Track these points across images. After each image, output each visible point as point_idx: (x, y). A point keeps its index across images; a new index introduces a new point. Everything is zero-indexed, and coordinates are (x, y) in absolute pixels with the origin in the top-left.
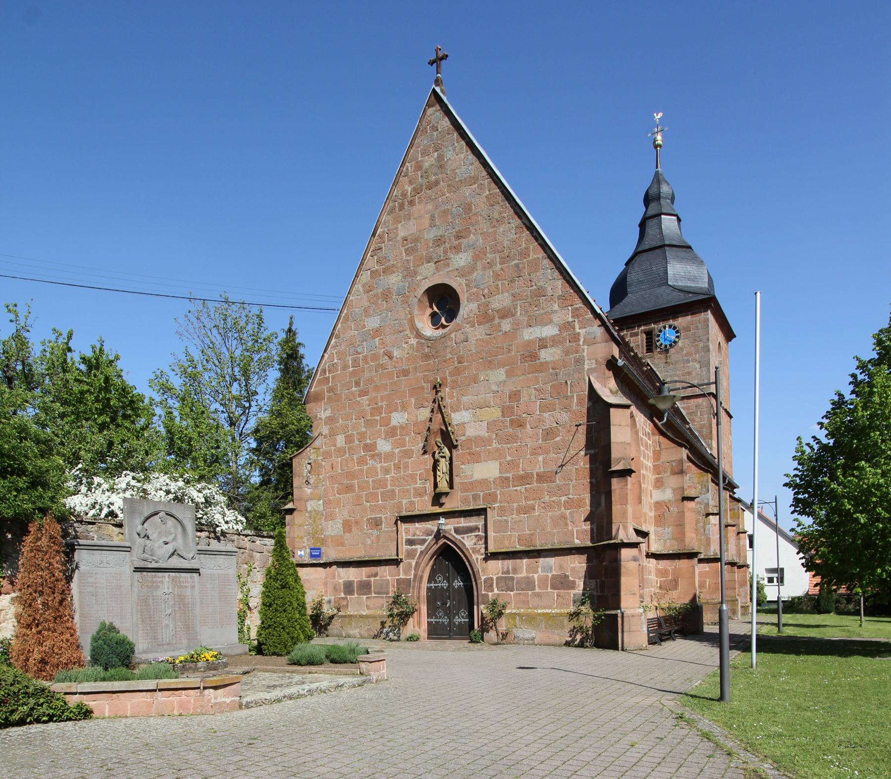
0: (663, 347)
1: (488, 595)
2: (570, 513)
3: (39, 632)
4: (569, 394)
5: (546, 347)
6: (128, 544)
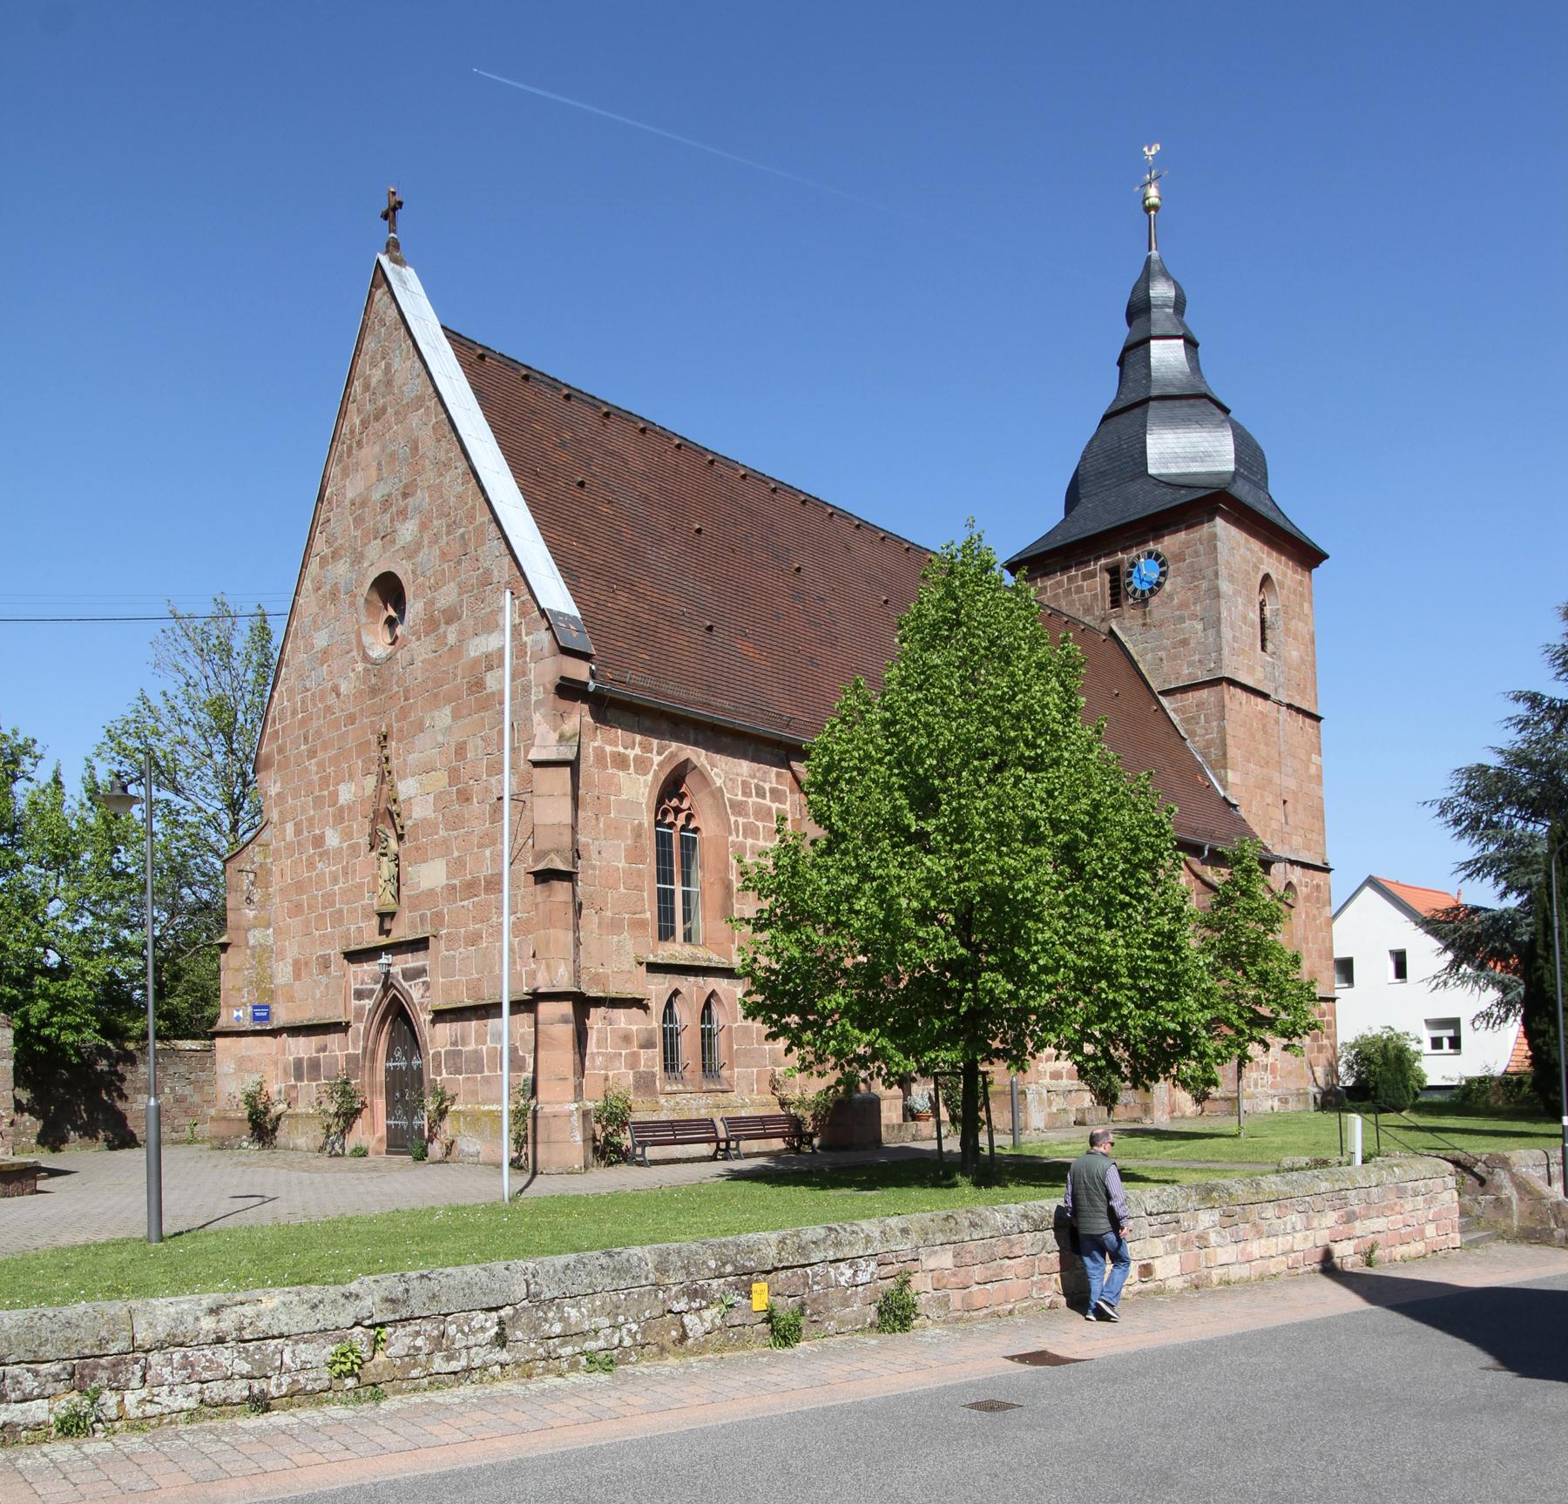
0: (1138, 594)
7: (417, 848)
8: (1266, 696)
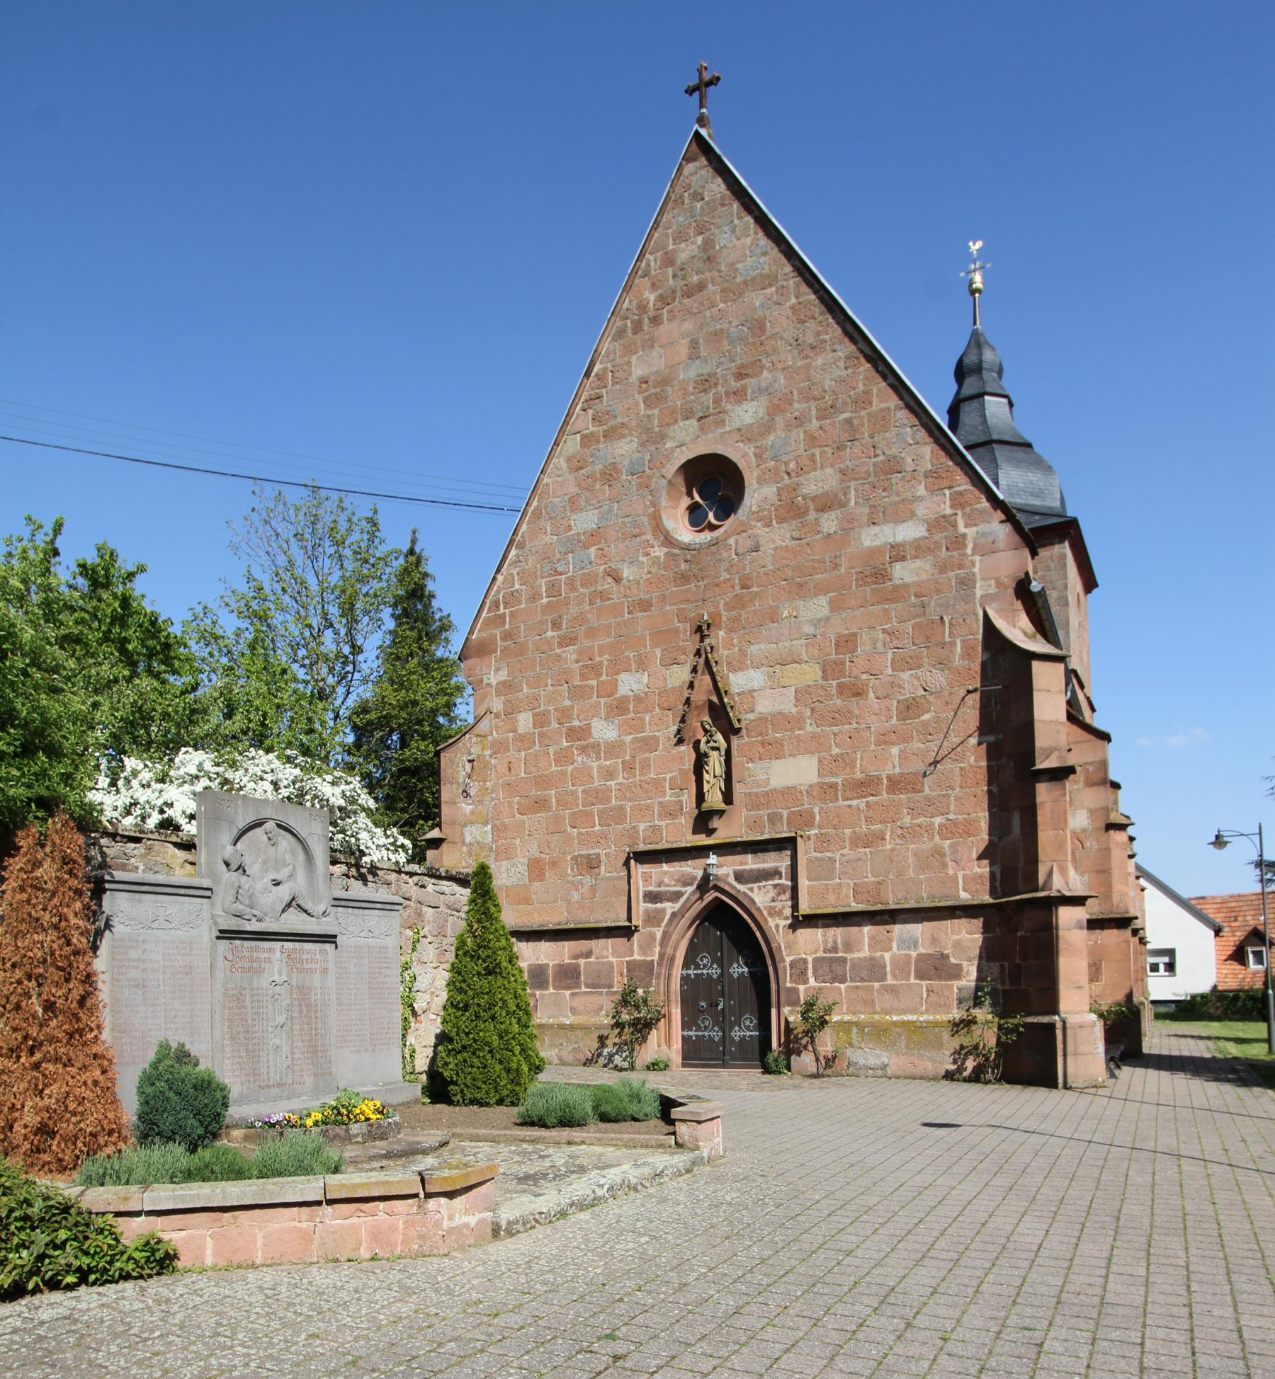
1: (797, 990)
2: (951, 846)
3: (36, 1066)
4: (947, 639)
5: (903, 559)
6: (206, 883)
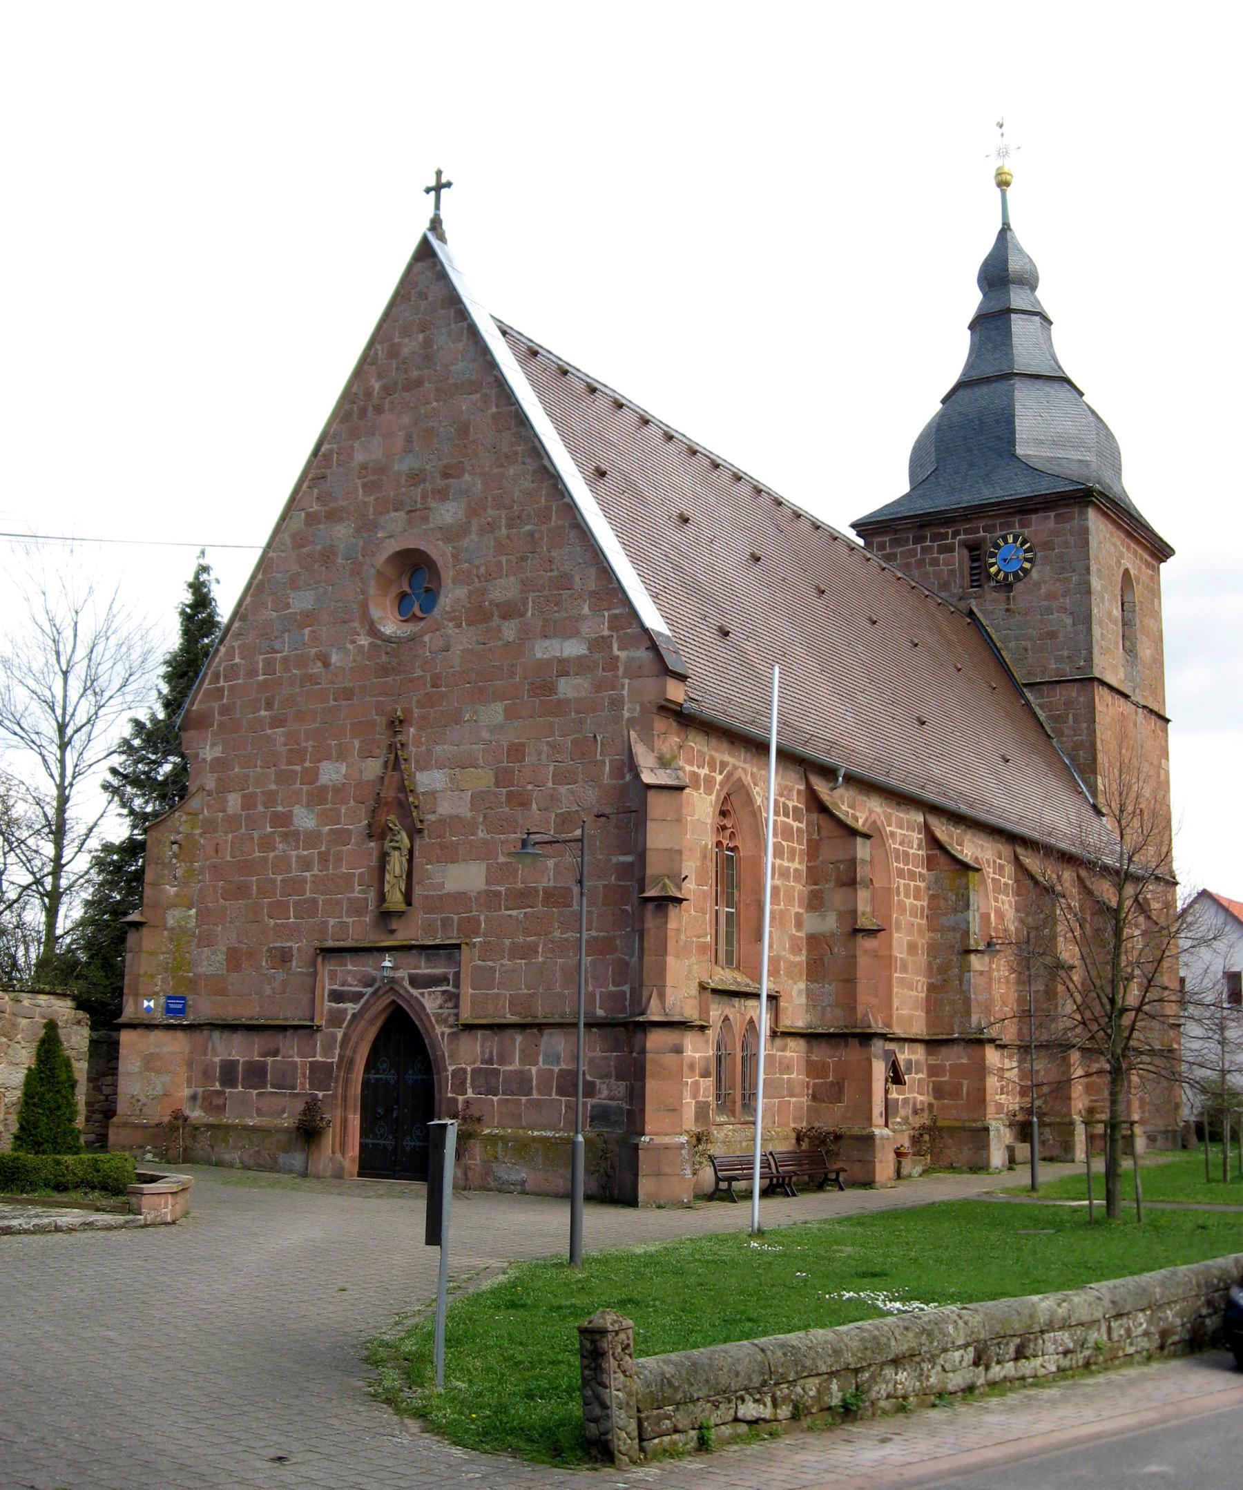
7: (442, 847)
8: (1126, 697)
